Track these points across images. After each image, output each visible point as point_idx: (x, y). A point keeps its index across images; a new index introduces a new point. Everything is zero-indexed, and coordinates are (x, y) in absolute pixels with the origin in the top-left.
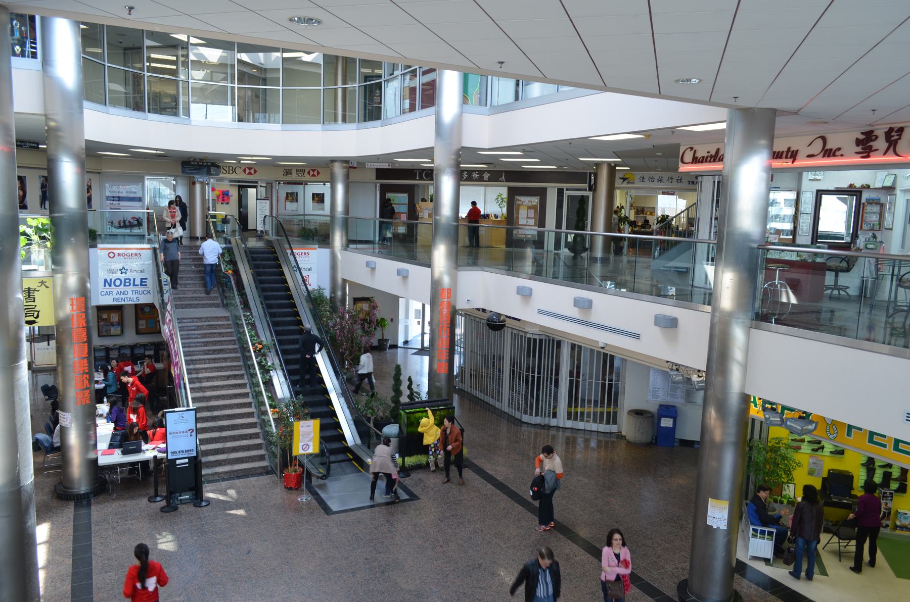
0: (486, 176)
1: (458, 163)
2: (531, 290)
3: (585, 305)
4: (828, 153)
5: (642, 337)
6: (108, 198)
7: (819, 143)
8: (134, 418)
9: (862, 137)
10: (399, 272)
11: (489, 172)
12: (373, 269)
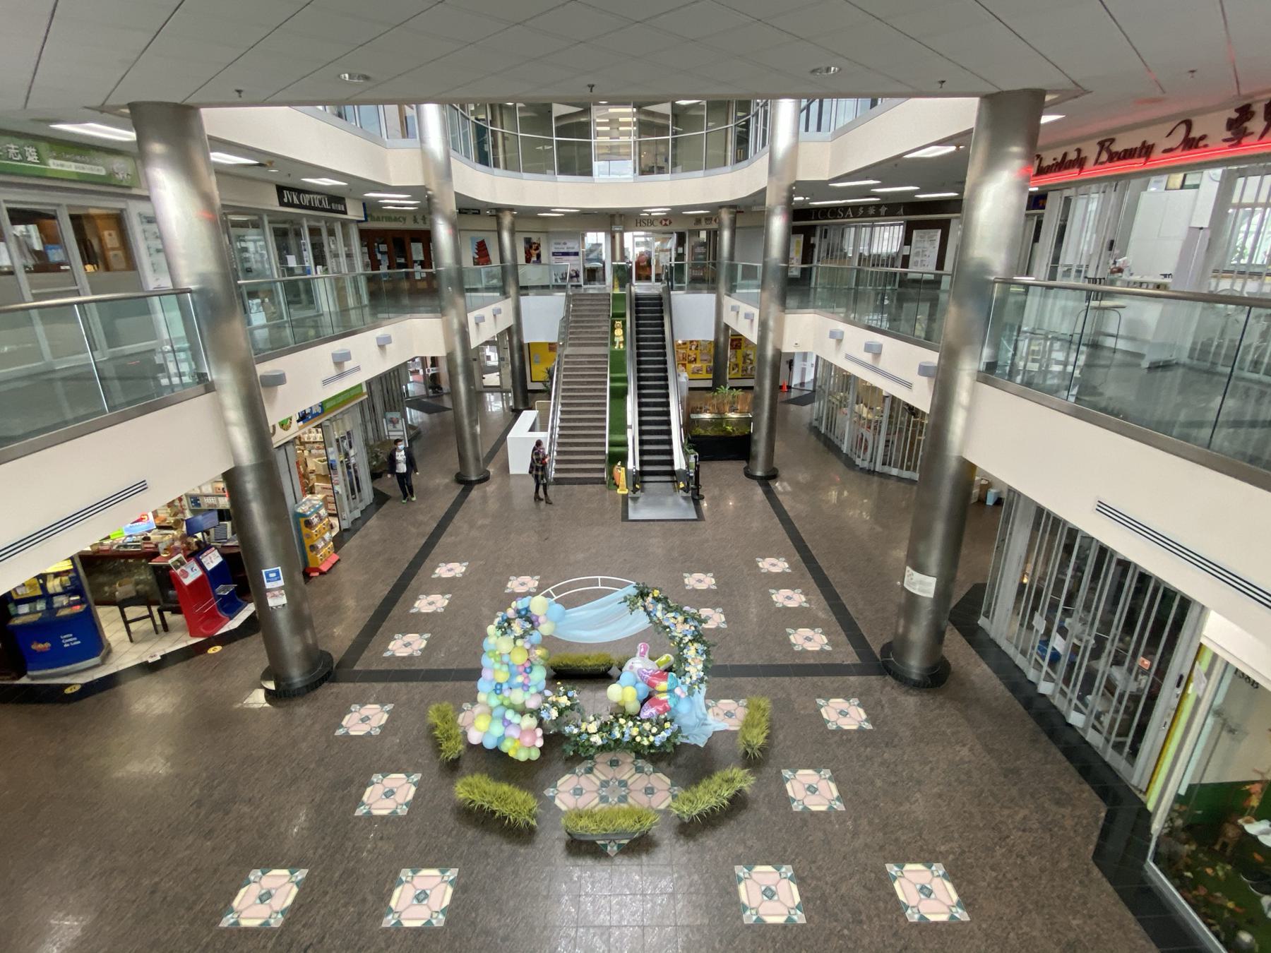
0: (883, 210)
1: (790, 199)
2: (881, 346)
3: (876, 351)
4: (1190, 143)
5: (914, 387)
6: (554, 254)
7: (1182, 130)
8: (1189, 874)
9: (1235, 115)
10: (832, 335)
11: (886, 205)
12: (839, 341)
